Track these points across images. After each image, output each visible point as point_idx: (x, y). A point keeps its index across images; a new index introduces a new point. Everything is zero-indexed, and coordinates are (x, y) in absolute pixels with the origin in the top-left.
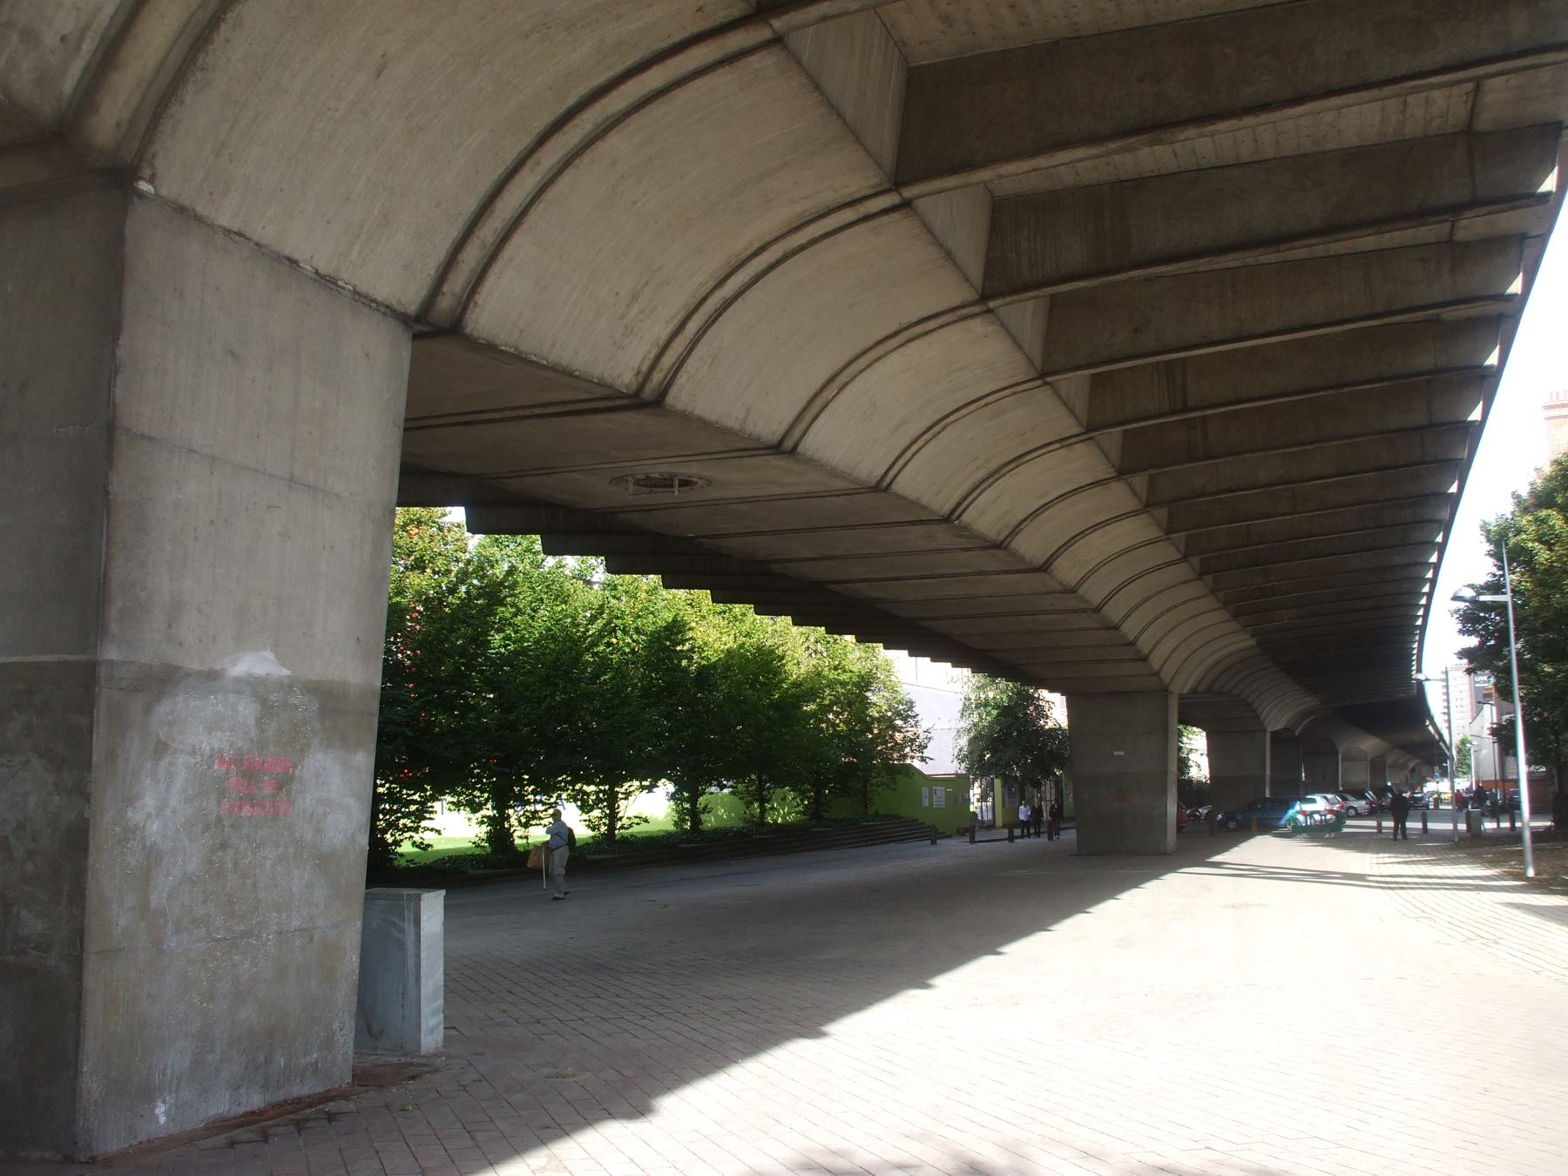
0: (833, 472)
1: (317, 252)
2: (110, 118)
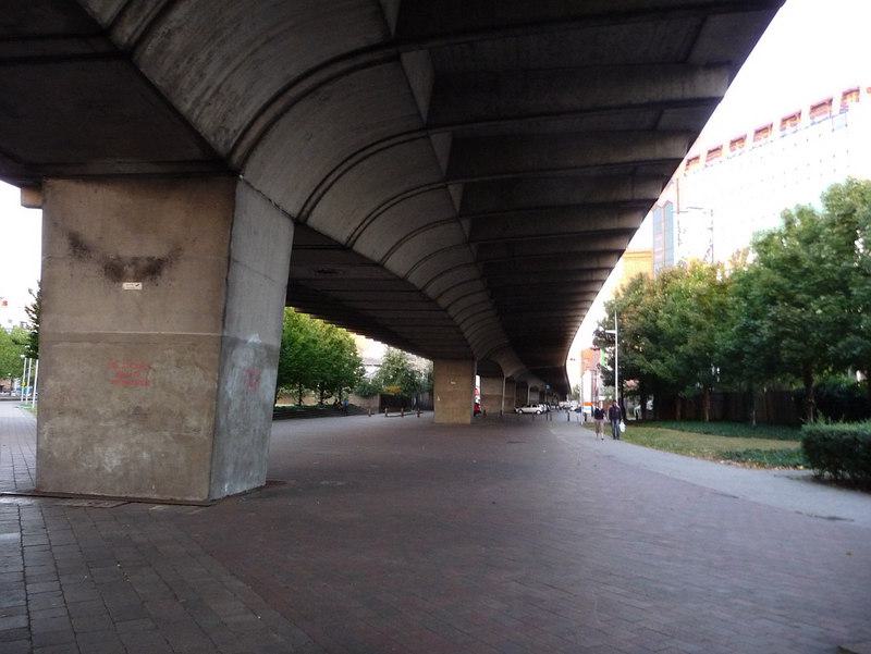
0: (392, 274)
1: (276, 198)
2: (236, 158)
